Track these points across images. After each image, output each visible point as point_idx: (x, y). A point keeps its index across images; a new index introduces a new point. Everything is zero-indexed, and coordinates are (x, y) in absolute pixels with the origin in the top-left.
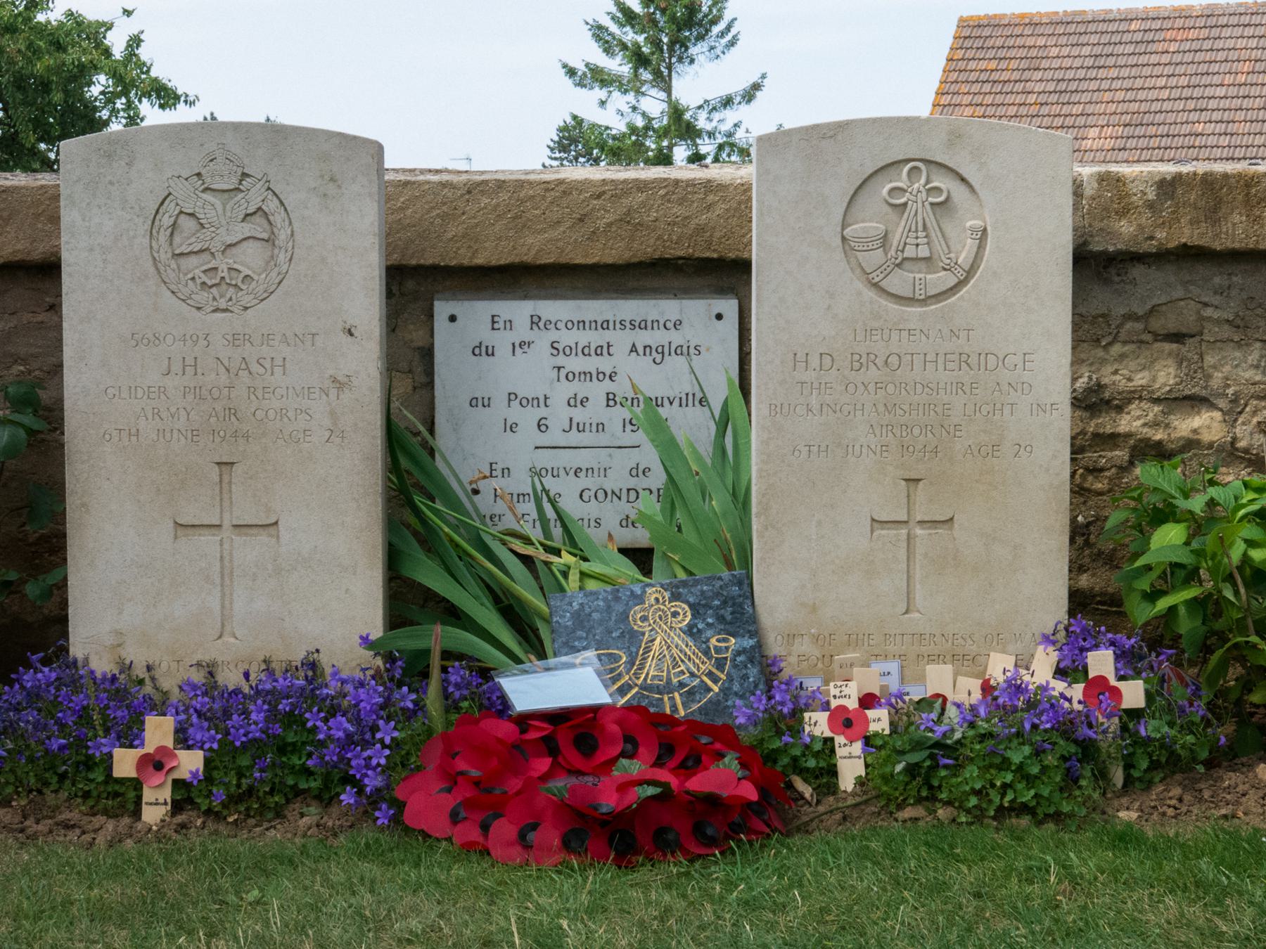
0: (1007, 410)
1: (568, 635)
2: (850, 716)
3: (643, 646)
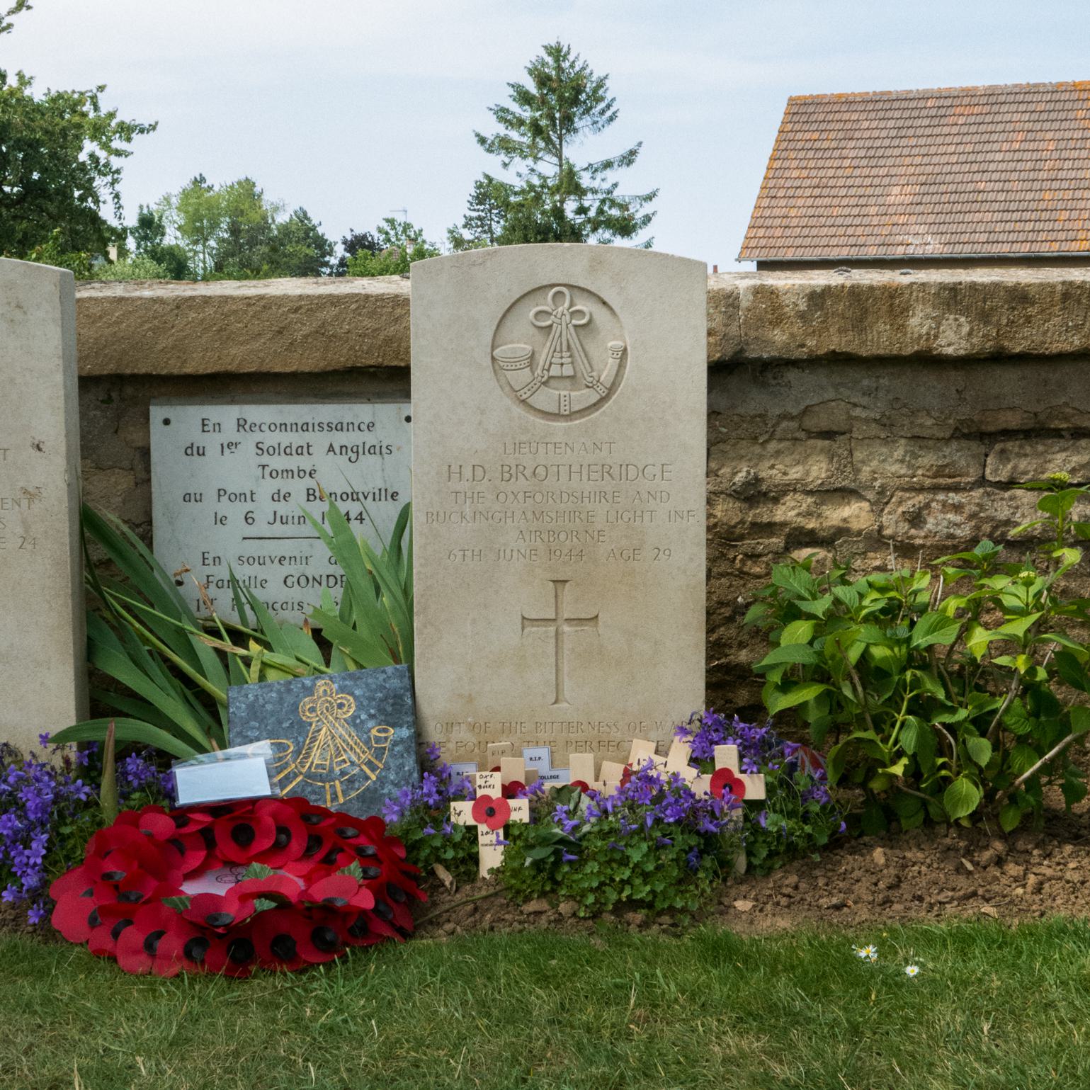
0: (647, 517)
1: (242, 725)
2: (493, 805)
3: (310, 736)
